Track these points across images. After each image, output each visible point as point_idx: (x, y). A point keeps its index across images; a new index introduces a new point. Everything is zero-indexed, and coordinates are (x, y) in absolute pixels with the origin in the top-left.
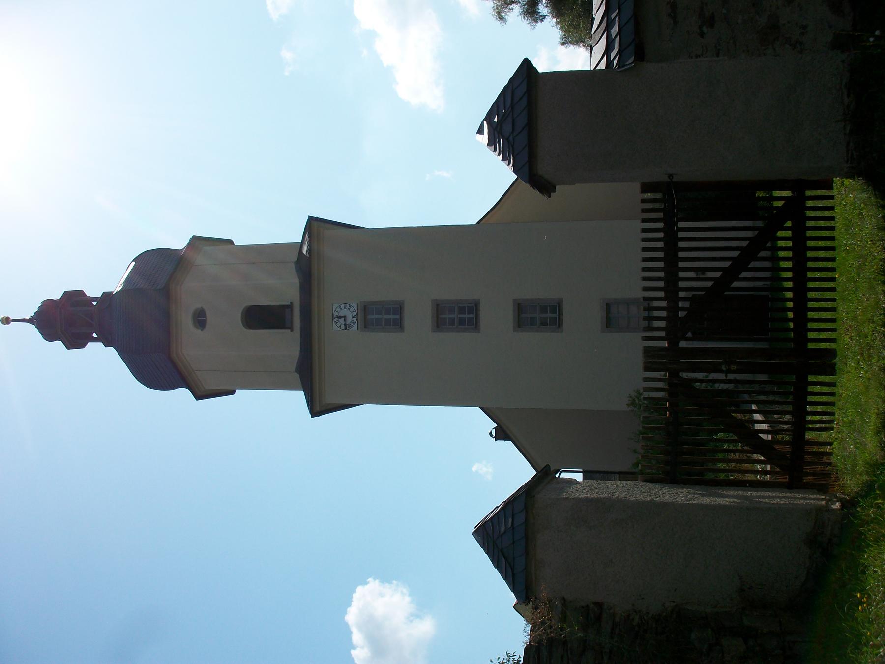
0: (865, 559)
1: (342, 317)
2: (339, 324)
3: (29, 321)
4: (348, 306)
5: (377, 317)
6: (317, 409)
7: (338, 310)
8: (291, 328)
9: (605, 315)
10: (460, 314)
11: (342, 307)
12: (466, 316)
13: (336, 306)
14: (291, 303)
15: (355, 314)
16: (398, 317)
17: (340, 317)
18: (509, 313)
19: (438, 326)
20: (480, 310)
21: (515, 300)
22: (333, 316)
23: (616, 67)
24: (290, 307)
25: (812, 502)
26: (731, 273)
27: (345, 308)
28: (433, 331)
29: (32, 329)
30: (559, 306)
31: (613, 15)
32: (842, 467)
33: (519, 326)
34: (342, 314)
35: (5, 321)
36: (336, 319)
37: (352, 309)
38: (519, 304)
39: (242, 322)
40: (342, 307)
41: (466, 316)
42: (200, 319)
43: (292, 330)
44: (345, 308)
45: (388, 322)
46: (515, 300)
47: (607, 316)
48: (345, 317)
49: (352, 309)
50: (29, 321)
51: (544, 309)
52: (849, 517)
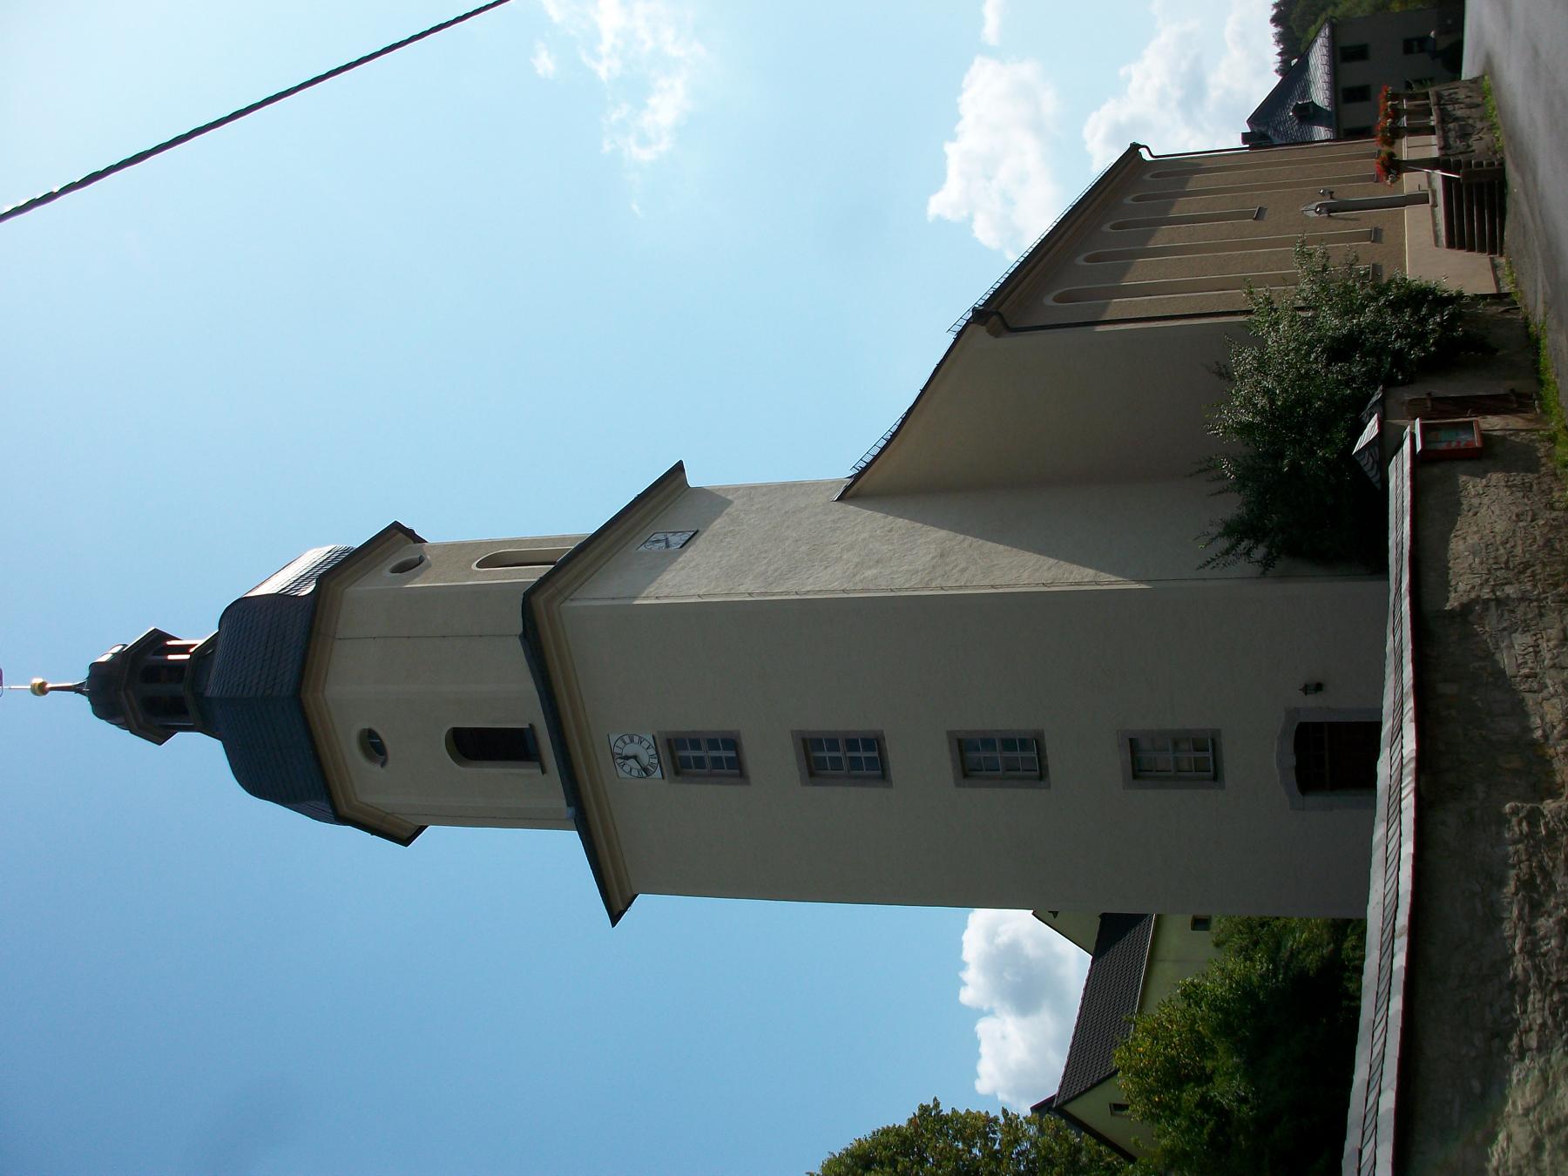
1: (631, 757)
2: (627, 768)
3: (77, 689)
4: (636, 739)
7: (620, 743)
9: (1130, 759)
13: (613, 738)
14: (530, 725)
15: (652, 752)
16: (732, 754)
17: (627, 758)
20: (886, 749)
21: (950, 734)
22: (613, 754)
23: (1386, 446)
27: (632, 741)
28: (739, 732)
29: (83, 703)
32: (845, 557)
33: (966, 776)
34: (631, 753)
35: (38, 692)
36: (619, 761)
37: (645, 744)
38: (960, 741)
39: (450, 754)
40: (627, 739)
42: (373, 746)
44: (632, 741)
45: (717, 762)
46: (950, 734)
47: (1132, 757)
48: (635, 757)
49: (645, 744)
50: (77, 689)
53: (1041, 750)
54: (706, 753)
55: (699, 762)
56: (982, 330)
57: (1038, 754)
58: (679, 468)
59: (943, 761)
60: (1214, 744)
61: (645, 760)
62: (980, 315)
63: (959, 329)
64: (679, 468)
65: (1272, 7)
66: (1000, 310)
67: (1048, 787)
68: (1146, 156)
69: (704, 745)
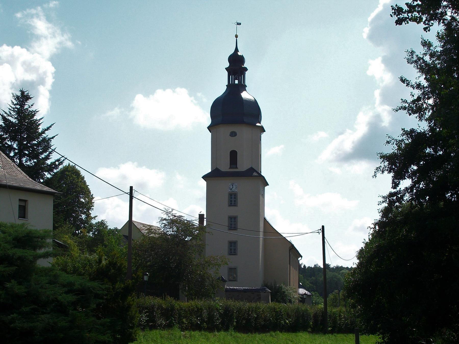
0: (212, 335)
2: (231, 185)
3: (237, 50)
5: (233, 202)
6: (209, 128)
7: (235, 185)
8: (230, 168)
10: (234, 224)
11: (236, 186)
12: (233, 197)
13: (236, 184)
17: (233, 186)
18: (232, 208)
19: (230, 217)
24: (237, 168)
25: (45, 189)
26: (129, 194)
27: (236, 187)
30: (236, 229)
31: (19, 161)
36: (232, 184)
37: (235, 189)
41: (233, 197)
42: (233, 134)
43: (229, 168)
44: (236, 187)
50: (237, 50)
51: (235, 250)
52: (63, 243)
53: (234, 255)
54: (233, 200)
55: (232, 198)
56: (290, 245)
57: (233, 254)
58: (269, 185)
59: (233, 239)
60: (235, 280)
61: (233, 189)
62: (293, 246)
63: (290, 242)
64: (269, 185)
65: (391, 11)
66: (293, 249)
67: (228, 255)
68: (299, 259)
69: (235, 199)
